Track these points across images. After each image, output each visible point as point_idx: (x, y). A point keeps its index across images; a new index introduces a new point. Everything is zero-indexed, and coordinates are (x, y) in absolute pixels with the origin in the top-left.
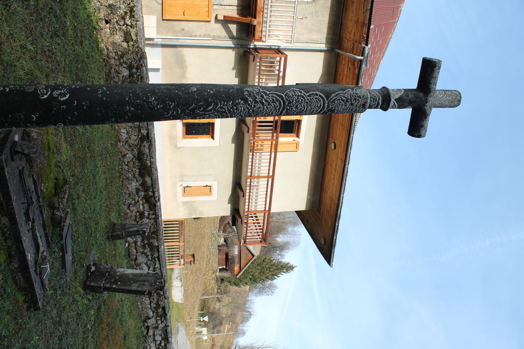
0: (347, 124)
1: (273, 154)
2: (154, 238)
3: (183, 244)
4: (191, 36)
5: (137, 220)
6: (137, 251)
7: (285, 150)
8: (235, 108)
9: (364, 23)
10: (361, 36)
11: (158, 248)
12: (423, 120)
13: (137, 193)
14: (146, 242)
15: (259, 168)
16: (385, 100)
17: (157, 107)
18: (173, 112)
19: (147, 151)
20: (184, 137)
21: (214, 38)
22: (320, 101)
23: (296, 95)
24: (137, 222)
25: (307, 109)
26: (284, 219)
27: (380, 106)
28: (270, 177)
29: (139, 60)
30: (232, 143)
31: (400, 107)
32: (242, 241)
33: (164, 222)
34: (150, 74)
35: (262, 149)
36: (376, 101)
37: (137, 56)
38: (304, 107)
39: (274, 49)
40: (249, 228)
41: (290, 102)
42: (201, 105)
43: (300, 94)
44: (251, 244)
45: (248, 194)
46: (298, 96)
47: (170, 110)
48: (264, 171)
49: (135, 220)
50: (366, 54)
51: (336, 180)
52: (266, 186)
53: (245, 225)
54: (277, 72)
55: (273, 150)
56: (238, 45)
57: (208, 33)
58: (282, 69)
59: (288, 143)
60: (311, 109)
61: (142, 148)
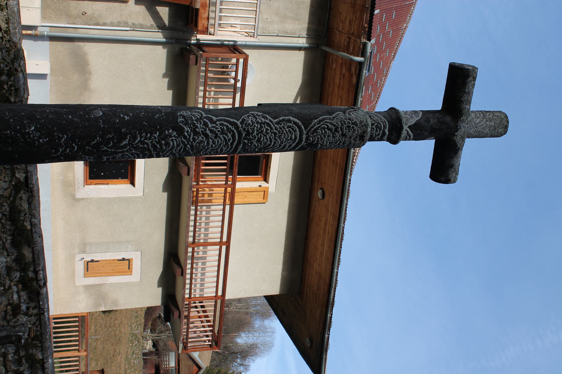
1: (228, 207)
2: (36, 347)
3: (85, 353)
4: (98, 24)
5: (8, 318)
6: (6, 369)
7: (246, 200)
8: (163, 142)
9: (364, 6)
11: (42, 363)
12: (452, 157)
13: (9, 274)
14: (22, 353)
15: (207, 229)
16: (393, 128)
17: (39, 142)
18: (66, 150)
19: (25, 206)
20: (86, 183)
21: (134, 27)
22: (295, 131)
23: (258, 123)
24: (8, 322)
26: (247, 309)
27: (386, 137)
28: (224, 244)
29: (13, 61)
30: (164, 191)
31: (416, 138)
32: (181, 346)
33: (54, 319)
34: (31, 84)
35: (210, 201)
36: (380, 130)
37: (9, 55)
38: (271, 141)
39: (227, 46)
40: (191, 325)
41: (248, 133)
42: (110, 139)
43: (263, 120)
44: (195, 349)
45: (188, 271)
46: (261, 124)
47: (60, 145)
48: (214, 235)
49: (5, 318)
50: (368, 54)
51: (326, 247)
52: (217, 258)
53: (186, 320)
54: (232, 81)
55: (228, 201)
56: (172, 38)
57: (124, 19)
58: (240, 77)
59: (194, 311)
60: (282, 142)
61: (18, 202)
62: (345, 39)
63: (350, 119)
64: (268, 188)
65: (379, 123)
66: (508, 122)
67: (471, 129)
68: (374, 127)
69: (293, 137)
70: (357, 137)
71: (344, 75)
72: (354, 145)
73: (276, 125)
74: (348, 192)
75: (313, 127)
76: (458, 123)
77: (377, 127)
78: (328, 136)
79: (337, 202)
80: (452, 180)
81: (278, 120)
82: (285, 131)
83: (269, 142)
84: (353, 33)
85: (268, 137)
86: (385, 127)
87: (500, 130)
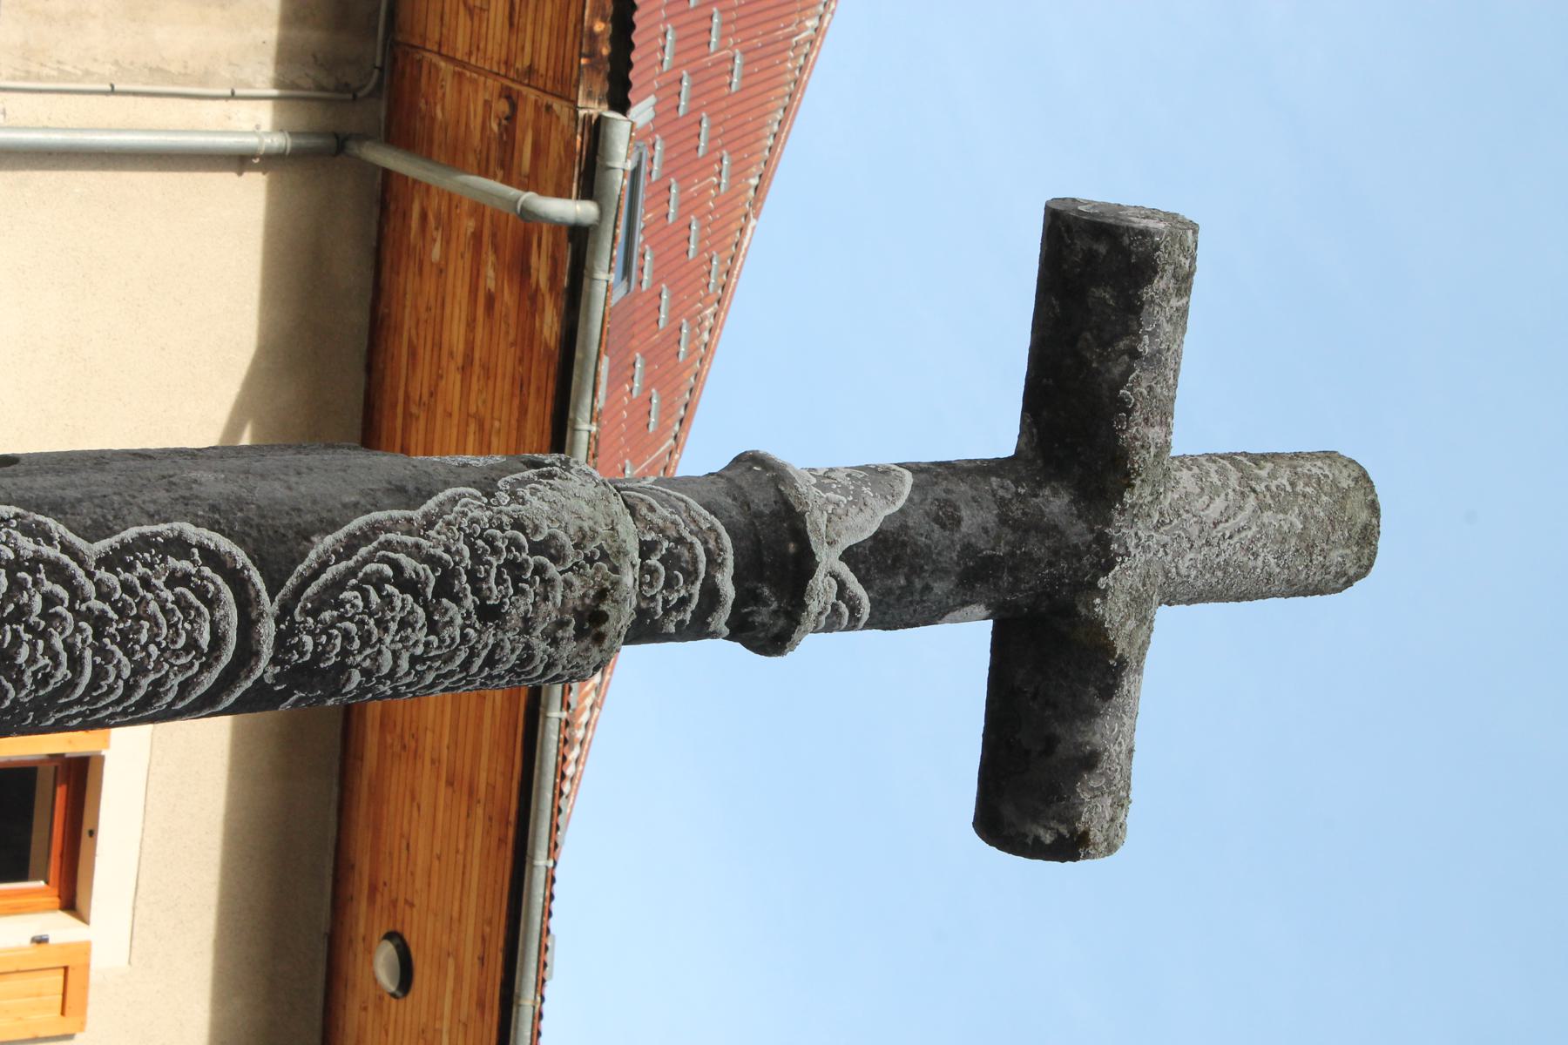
0: (492, 771)
10: (572, 31)
12: (1091, 714)
16: (763, 570)
22: (212, 603)
25: (99, 673)
31: (888, 616)
36: (691, 576)
38: (76, 663)
43: (28, 546)
50: (619, 181)
60: (139, 670)
62: (487, 104)
63: (518, 525)
64: (85, 949)
65: (680, 540)
66: (1374, 508)
67: (1180, 554)
68: (653, 561)
69: (205, 640)
70: (562, 624)
71: (491, 300)
72: (549, 666)
73: (102, 574)
74: (543, 949)
75: (315, 575)
76: (1108, 522)
77: (670, 560)
78: (403, 624)
79: (481, 1004)
80: (1096, 835)
81: (113, 541)
82: (154, 607)
83: (63, 672)
84: (531, 70)
85: (57, 642)
86: (713, 562)
87: (1335, 556)
